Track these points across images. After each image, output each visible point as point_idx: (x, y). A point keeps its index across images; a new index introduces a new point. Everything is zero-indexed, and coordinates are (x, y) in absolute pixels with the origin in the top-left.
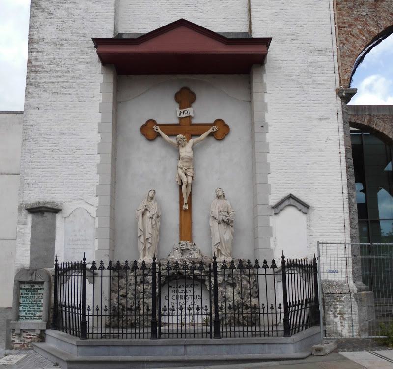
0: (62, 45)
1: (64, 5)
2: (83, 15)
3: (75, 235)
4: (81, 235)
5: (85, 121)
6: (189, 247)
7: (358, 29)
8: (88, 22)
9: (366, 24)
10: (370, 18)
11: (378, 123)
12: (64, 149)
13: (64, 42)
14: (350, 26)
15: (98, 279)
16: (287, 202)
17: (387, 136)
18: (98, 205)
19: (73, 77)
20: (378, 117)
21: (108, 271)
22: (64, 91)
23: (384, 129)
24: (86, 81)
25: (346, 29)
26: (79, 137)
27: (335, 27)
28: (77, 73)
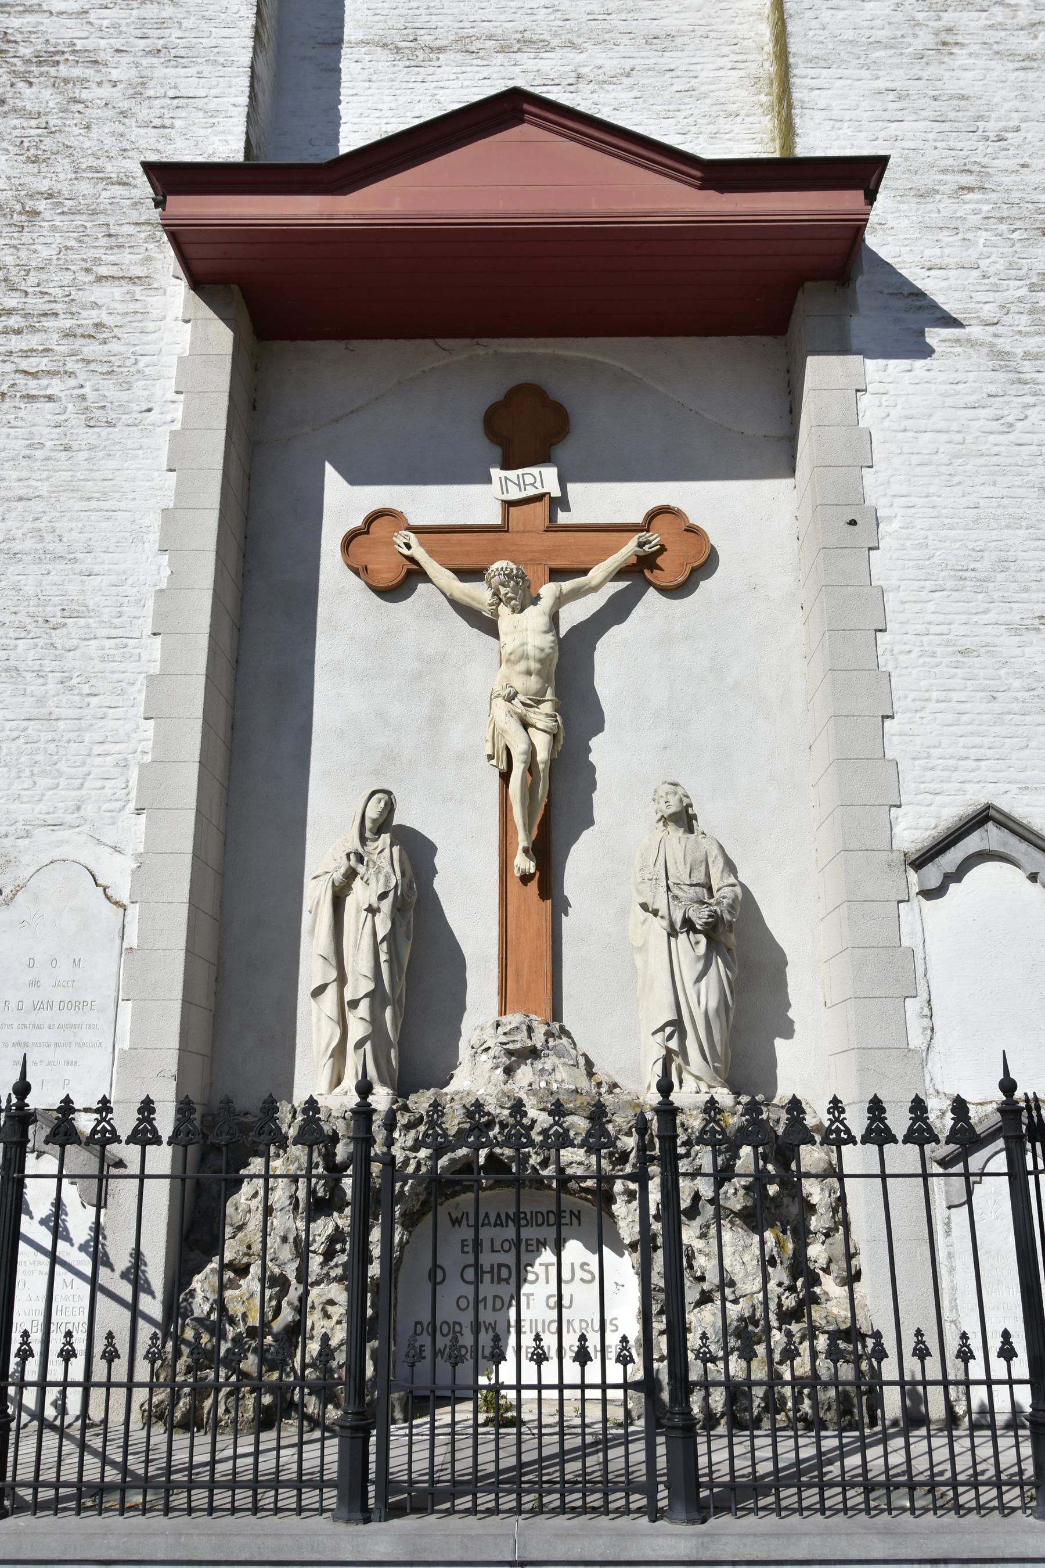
0: (36, 213)
1: (53, 71)
2: (125, 105)
3: (34, 983)
4: (58, 984)
5: (106, 505)
6: (538, 1040)
8: (142, 131)
12: (13, 618)
13: (42, 205)
15: (123, 1191)
16: (972, 843)
18: (141, 849)
19: (69, 334)
21: (913, 1149)
22: (33, 386)
24: (122, 349)
26: (77, 567)
28: (88, 318)
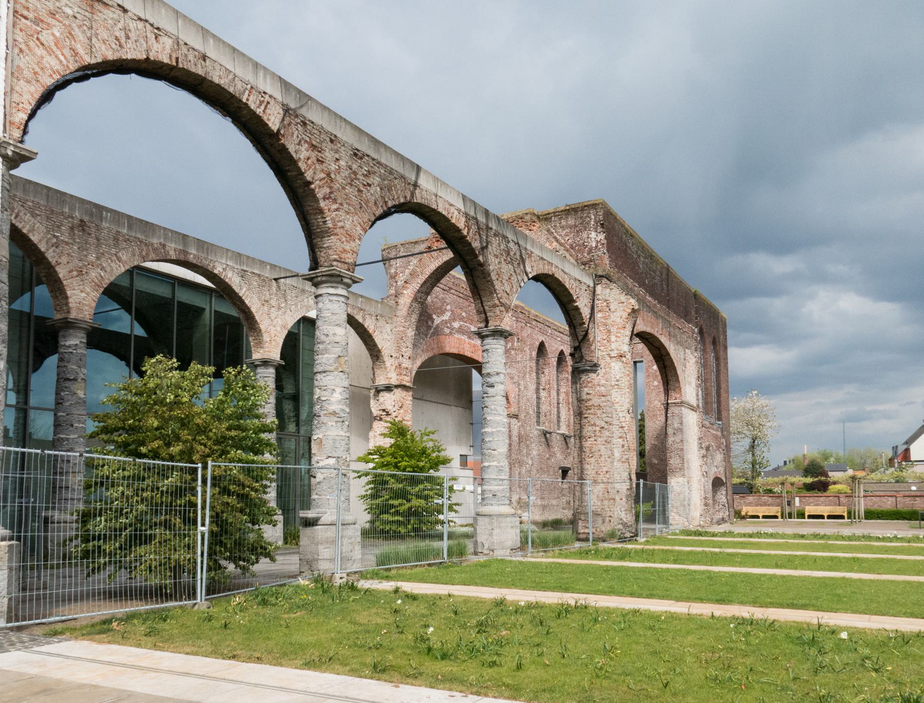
7: (53, 35)
9: (70, 34)
10: (80, 27)
11: (21, 214)
14: (38, 21)
17: (35, 245)
20: (23, 203)
23: (32, 230)
25: (28, 22)
27: (8, 8)
